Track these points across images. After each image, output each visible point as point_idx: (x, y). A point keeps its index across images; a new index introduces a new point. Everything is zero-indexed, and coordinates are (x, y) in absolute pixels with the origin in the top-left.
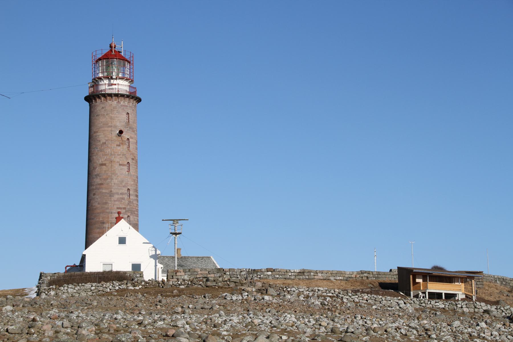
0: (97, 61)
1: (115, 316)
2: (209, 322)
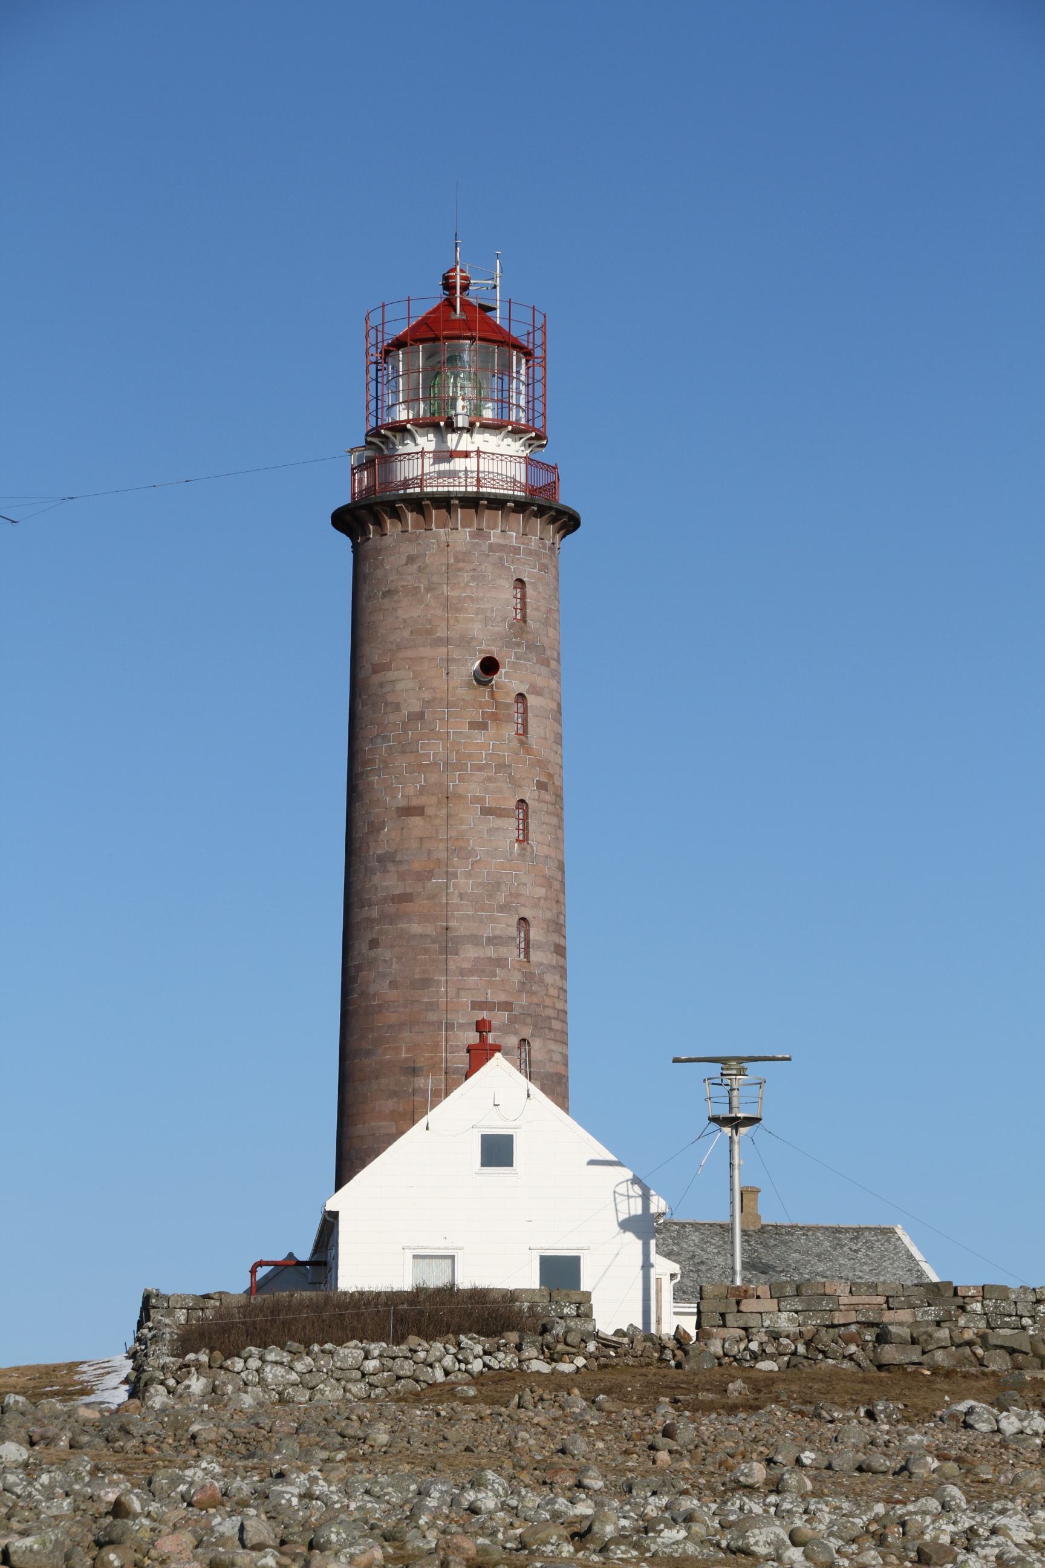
0: (387, 352)
1: (470, 1496)
2: (894, 1534)
